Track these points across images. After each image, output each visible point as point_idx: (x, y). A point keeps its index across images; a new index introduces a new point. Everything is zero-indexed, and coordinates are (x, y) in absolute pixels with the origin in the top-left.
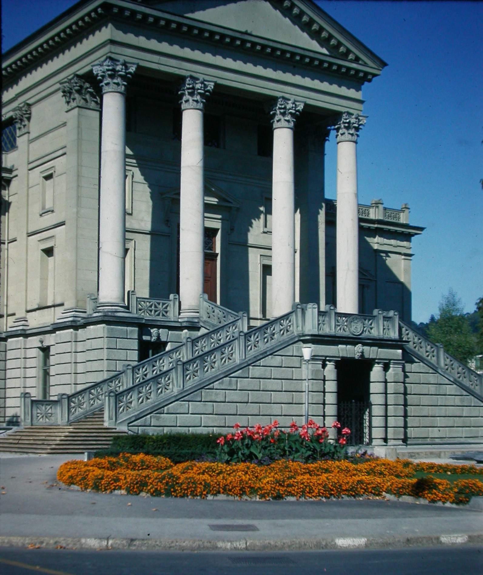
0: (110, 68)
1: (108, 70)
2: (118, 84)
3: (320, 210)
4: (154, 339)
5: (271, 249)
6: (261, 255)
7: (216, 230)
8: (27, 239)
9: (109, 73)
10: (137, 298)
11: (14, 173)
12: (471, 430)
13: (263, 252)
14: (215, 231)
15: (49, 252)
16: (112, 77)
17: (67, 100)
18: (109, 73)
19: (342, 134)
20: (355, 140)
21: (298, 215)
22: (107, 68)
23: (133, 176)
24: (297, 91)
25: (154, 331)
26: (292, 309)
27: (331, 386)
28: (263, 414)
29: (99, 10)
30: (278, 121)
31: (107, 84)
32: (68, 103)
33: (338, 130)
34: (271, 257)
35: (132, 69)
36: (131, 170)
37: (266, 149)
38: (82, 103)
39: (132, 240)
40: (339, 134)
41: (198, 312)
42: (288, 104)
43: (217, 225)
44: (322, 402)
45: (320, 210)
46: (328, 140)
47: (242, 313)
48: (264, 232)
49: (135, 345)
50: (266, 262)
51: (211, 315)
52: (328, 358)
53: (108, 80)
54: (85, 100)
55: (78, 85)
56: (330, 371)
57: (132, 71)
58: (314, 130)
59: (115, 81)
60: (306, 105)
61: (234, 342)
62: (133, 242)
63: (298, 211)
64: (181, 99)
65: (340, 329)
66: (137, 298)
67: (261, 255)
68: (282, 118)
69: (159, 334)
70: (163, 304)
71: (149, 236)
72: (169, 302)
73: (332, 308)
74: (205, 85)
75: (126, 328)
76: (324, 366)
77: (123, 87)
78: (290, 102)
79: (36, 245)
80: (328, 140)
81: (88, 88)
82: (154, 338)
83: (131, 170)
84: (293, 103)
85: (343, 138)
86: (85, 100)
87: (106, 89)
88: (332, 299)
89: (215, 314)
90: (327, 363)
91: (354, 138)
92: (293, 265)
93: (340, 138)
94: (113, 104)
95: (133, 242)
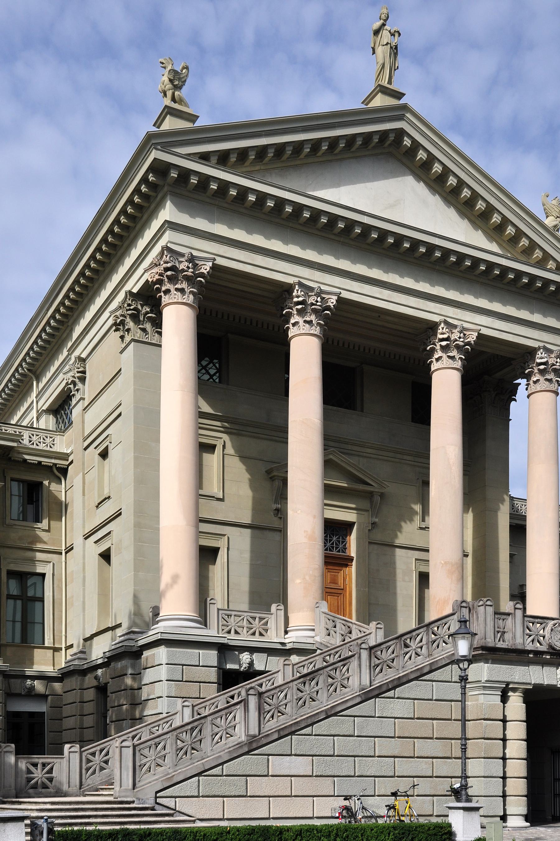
0: (169, 265)
1: (166, 269)
2: (182, 291)
3: (501, 505)
4: (245, 666)
5: (428, 551)
6: (416, 559)
7: (350, 525)
8: (84, 544)
9: (169, 273)
10: (218, 610)
11: (70, 459)
12: (478, 743)
13: (417, 555)
14: (347, 527)
15: (106, 556)
16: (172, 280)
17: (122, 334)
18: (169, 273)
19: (535, 382)
20: (554, 389)
21: (470, 517)
22: (165, 265)
23: (224, 447)
24: (469, 317)
25: (245, 657)
26: (453, 610)
27: (517, 731)
28: (275, 816)
29: (151, 178)
30: (438, 360)
31: (167, 292)
32: (122, 337)
33: (528, 377)
34: (428, 561)
35: (206, 268)
36: (221, 438)
37: (421, 413)
38: (139, 335)
39: (224, 535)
40: (531, 382)
41: (313, 630)
42: (452, 333)
43: (349, 516)
44: (501, 755)
45: (501, 505)
46: (515, 400)
47: (375, 623)
48: (421, 528)
49: (213, 675)
50: (423, 569)
51: (332, 632)
52: (511, 686)
53: (167, 286)
54: (144, 330)
55: (132, 307)
56: (516, 707)
57: (205, 272)
58: (492, 378)
59: (178, 286)
60: (481, 337)
61: (350, 660)
62: (226, 537)
63: (471, 509)
64: (288, 322)
65: (533, 641)
66: (218, 610)
67: (416, 559)
68: (444, 356)
69: (252, 661)
70: (261, 619)
71: (248, 531)
72: (269, 616)
73: (519, 606)
74: (323, 299)
75: (197, 651)
76: (504, 699)
77: (191, 297)
78: (455, 331)
79: (93, 550)
80: (515, 400)
81: (147, 313)
82: (244, 666)
83: (221, 438)
84: (461, 332)
85: (538, 387)
86: (144, 330)
87: (165, 299)
88: (519, 595)
89: (337, 628)
90: (510, 694)
91: (554, 386)
92: (460, 569)
93: (533, 388)
94: (178, 321)
95: (226, 537)
